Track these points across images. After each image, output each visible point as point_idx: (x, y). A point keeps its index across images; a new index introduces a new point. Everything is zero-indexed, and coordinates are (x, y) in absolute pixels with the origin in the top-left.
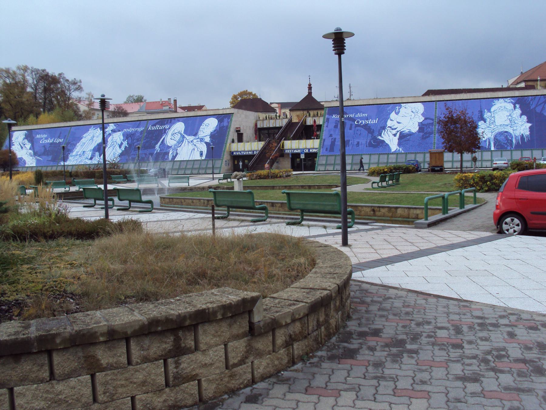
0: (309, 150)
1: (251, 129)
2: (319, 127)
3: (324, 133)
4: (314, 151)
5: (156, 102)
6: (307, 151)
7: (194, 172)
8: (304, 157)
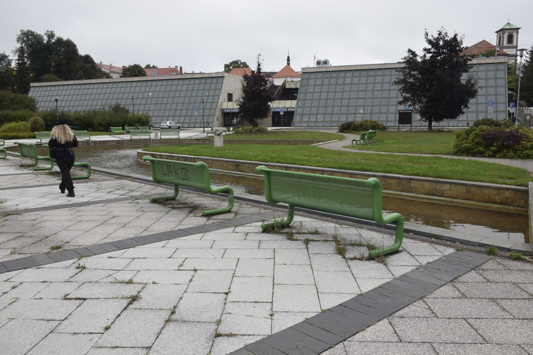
0: (287, 109)
3: (300, 96)
4: (292, 110)
6: (286, 110)
7: (191, 125)
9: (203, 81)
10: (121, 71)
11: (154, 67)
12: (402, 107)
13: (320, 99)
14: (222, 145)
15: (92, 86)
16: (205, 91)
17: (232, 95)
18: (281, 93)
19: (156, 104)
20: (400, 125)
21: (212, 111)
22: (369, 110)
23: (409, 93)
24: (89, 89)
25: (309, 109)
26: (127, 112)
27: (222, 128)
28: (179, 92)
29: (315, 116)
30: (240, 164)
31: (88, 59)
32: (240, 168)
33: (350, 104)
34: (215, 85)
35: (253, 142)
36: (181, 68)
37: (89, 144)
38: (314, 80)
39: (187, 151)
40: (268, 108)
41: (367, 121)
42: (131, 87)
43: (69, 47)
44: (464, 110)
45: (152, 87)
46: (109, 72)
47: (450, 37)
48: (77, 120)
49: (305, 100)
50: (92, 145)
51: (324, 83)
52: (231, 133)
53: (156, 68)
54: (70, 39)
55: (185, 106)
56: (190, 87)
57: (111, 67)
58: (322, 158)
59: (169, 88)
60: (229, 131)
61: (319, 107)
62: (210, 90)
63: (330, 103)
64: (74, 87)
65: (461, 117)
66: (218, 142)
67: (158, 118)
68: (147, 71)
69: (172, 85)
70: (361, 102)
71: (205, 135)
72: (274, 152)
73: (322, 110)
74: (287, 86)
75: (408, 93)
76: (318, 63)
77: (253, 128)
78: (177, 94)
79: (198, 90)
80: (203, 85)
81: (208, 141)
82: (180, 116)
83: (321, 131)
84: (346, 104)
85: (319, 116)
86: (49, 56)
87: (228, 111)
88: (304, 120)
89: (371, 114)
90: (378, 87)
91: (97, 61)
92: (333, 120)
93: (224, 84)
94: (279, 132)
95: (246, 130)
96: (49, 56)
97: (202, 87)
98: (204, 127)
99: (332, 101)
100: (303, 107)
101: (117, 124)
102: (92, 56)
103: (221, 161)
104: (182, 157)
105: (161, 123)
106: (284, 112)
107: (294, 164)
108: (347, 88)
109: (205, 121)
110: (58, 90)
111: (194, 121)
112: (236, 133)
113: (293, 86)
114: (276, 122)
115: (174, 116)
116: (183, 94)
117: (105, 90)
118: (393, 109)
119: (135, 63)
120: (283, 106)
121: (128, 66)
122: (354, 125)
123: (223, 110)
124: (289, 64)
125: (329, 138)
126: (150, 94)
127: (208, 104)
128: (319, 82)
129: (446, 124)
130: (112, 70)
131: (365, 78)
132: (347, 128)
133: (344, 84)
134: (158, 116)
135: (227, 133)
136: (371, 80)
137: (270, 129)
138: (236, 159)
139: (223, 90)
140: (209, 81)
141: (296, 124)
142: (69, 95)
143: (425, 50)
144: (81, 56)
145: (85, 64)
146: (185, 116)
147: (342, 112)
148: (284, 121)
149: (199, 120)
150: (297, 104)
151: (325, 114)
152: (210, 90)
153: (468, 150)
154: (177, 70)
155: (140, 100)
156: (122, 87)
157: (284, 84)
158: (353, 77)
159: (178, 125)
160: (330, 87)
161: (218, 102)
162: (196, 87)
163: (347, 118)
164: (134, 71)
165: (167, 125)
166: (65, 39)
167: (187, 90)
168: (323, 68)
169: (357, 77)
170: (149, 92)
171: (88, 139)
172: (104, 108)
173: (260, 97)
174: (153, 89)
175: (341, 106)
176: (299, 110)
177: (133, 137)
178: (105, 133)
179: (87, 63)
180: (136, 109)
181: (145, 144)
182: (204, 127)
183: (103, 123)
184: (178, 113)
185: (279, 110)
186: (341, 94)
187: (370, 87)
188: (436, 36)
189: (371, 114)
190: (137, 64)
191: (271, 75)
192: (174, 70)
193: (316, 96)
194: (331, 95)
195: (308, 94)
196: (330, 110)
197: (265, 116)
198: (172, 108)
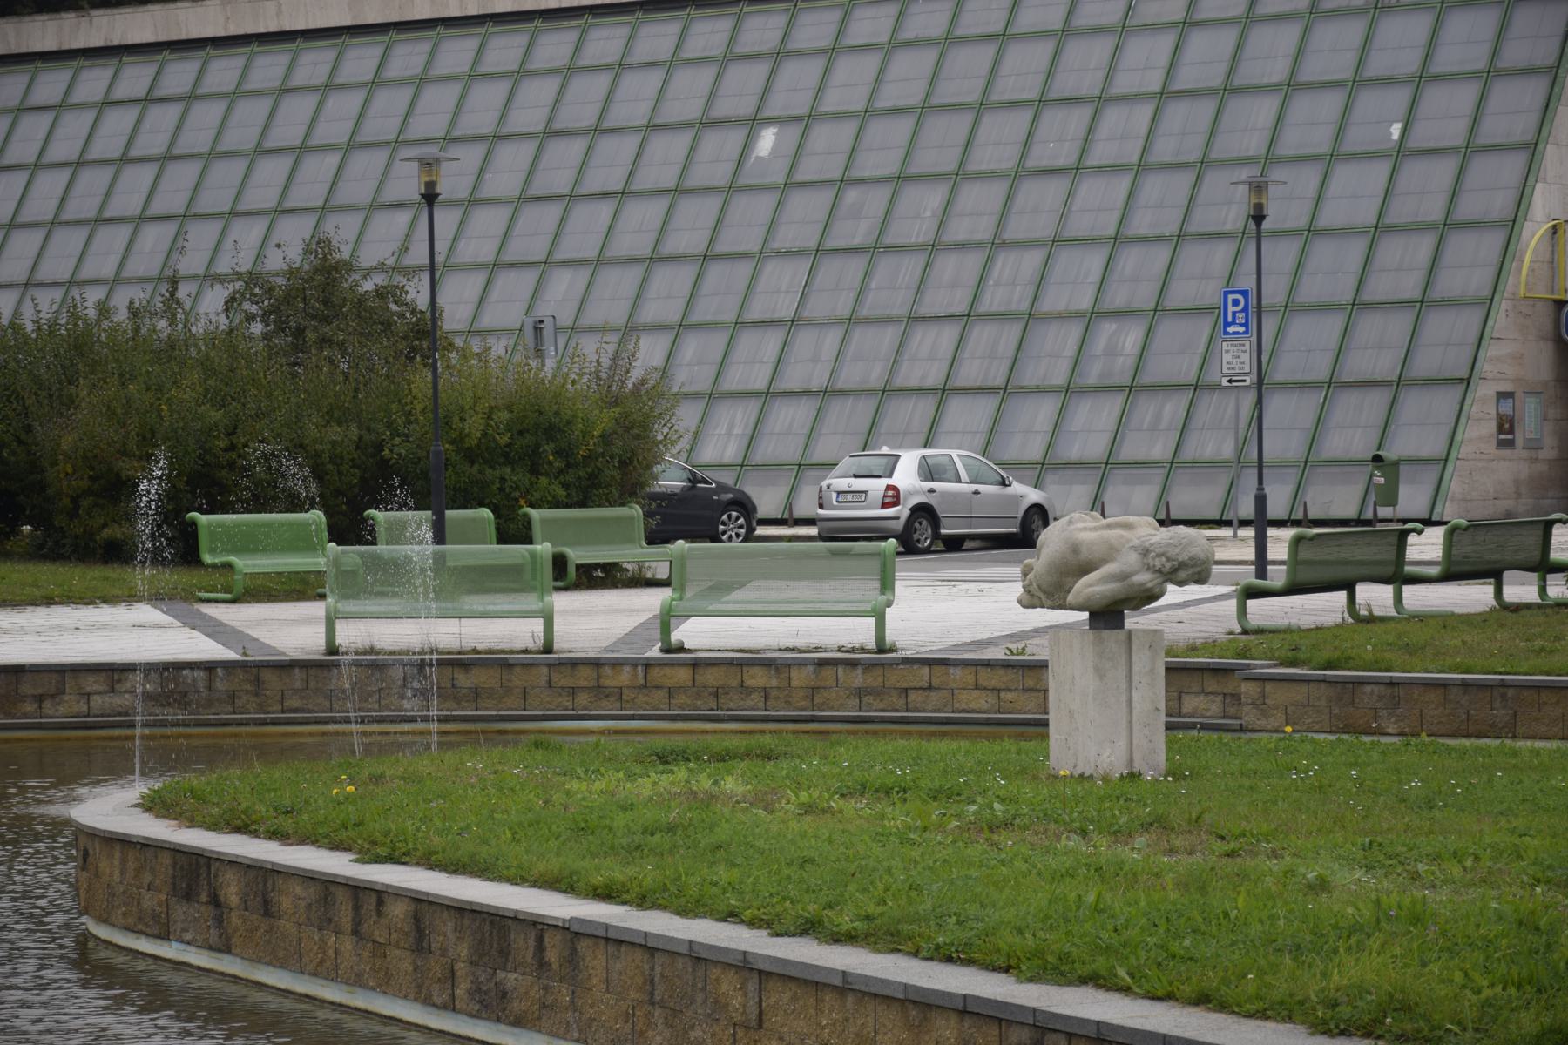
14: (1151, 750)
16: (1368, 102)
19: (820, 252)
26: (425, 335)
62: (1423, 79)
66: (1102, 725)
79: (1292, 86)
82: (1070, 391)
101: (435, 490)
104: (461, 910)
116: (1121, 132)
126: (767, 140)
134: (828, 393)
135: (1521, 589)
146: (1133, 389)
152: (1423, 79)
155: (931, 199)
161: (1512, 225)
165: (893, 497)
167: (1165, 95)
170: (755, 123)
177: (350, 635)
180: (512, 305)
184: (1052, 354)
198: (1181, 294)
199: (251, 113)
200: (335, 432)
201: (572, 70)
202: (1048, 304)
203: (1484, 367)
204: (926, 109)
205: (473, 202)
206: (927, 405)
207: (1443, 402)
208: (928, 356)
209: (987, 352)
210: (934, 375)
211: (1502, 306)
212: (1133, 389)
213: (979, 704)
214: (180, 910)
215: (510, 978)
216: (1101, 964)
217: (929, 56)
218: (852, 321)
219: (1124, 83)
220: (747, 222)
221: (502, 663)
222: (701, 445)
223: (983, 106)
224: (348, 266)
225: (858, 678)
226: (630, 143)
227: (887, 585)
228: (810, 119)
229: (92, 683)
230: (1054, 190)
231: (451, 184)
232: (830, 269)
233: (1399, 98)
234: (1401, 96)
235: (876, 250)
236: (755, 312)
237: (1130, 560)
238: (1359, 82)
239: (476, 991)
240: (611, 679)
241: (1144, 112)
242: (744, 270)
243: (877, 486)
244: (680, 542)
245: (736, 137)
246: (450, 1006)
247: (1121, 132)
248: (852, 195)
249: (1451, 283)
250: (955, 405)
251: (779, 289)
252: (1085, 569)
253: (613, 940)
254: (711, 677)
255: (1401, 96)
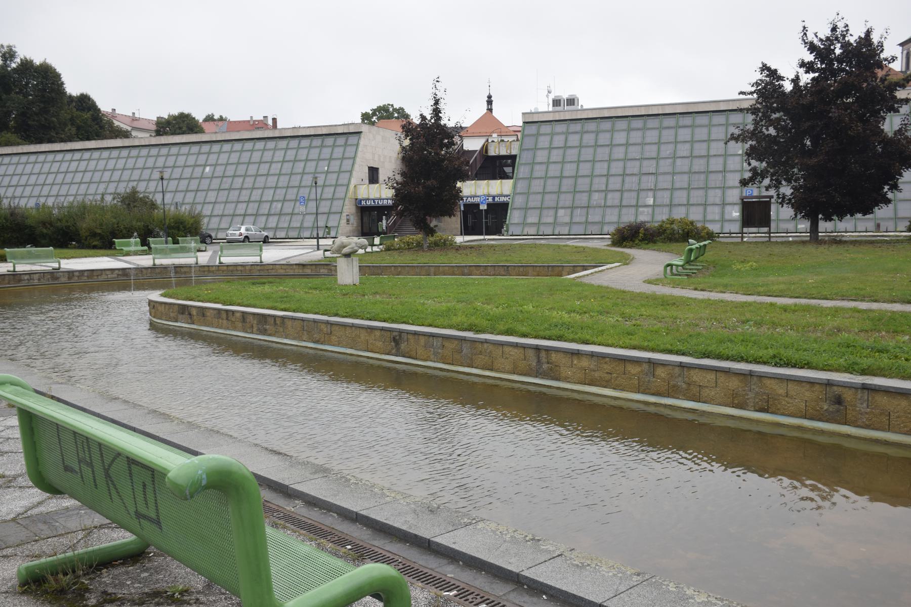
0: (494, 198)
1: (393, 161)
2: (513, 158)
3: (522, 170)
4: (502, 199)
5: (244, 122)
6: (490, 199)
7: (291, 234)
8: (485, 207)
9: (317, 142)
10: (154, 128)
11: (221, 119)
12: (753, 191)
13: (561, 177)
14: (357, 280)
15: (87, 155)
16: (321, 163)
17: (377, 169)
18: (479, 166)
20: (745, 230)
21: (335, 203)
22: (665, 197)
23: (761, 161)
24: (80, 160)
25: (539, 197)
26: (153, 205)
27: (356, 239)
28: (267, 165)
29: (552, 212)
30: (404, 336)
31: (85, 102)
32: (403, 346)
33: (627, 187)
34: (341, 149)
35: (426, 270)
36: (274, 120)
37: (57, 278)
38: (548, 138)
39: (268, 298)
40: (456, 195)
41: (672, 222)
42: (168, 155)
43: (47, 77)
44: (890, 195)
45: (211, 156)
46: (129, 129)
47: (856, 37)
48: (44, 223)
49: (531, 178)
50: (64, 279)
51: (569, 144)
52: (375, 249)
53: (225, 120)
54: (49, 61)
55: (280, 194)
56: (291, 155)
57: (134, 119)
58: (623, 315)
59: (245, 157)
60: (373, 245)
61: (559, 192)
62: (331, 159)
63: (583, 184)
64: (50, 157)
65: (882, 212)
66: (347, 274)
67: (224, 219)
68: (207, 127)
69: (252, 151)
70: (648, 182)
71: (319, 255)
72: (489, 300)
73: (566, 200)
74: (492, 152)
75: (761, 160)
76: (556, 102)
77: (425, 239)
78: (264, 169)
79: (307, 160)
80: (318, 150)
81: (325, 268)
82: (268, 215)
83: (570, 243)
84: (618, 187)
85: (561, 212)
86: (4, 96)
87: (368, 203)
88: (529, 220)
89: (671, 206)
90: (684, 150)
91: (104, 106)
92: (590, 219)
93: (360, 149)
94: (480, 246)
95: (408, 244)
96: (4, 96)
97: (314, 153)
98: (318, 238)
99: (588, 180)
100: (528, 194)
102: (94, 96)
103: (353, 326)
104: (254, 314)
105: (228, 229)
106: (488, 205)
107: (560, 338)
108: (619, 153)
109: (321, 223)
110: (18, 164)
111: (298, 225)
112: (388, 249)
113: (503, 152)
114: (470, 224)
115: (256, 215)
116: (275, 168)
117: (114, 161)
118: (734, 195)
119: (181, 111)
120: (485, 192)
121: (166, 117)
122: (646, 230)
123: (358, 201)
124: (490, 110)
125: (597, 260)
126: (208, 169)
127: (327, 190)
128: (559, 141)
129: (851, 226)
130: (136, 124)
131: (655, 133)
132: (631, 236)
133: (611, 145)
134: (222, 216)
135: (369, 249)
136: (668, 135)
137: (459, 239)
138: (393, 322)
139: (358, 160)
140: (329, 141)
141: (512, 229)
142: (39, 174)
143: (803, 64)
144: (70, 96)
145: (79, 113)
146: (280, 215)
147: (609, 203)
148: (486, 223)
149: (309, 221)
150: (515, 186)
151: (573, 208)
152: (331, 159)
153: (444, 243)
154: (266, 125)
155: (185, 182)
156: (148, 156)
157: (485, 148)
158: (629, 130)
159: (266, 234)
160: (583, 150)
161: (348, 185)
162: (303, 154)
163: (620, 216)
164: (180, 124)
165: (241, 234)
166: (37, 61)
167: (283, 162)
168: (567, 113)
169: (639, 129)
170: (205, 166)
171: (56, 265)
172: (102, 199)
173: (435, 178)
174: (213, 159)
175: (607, 191)
176: (519, 201)
177: (158, 262)
178: (102, 251)
179: (83, 110)
180: (173, 199)
181: (181, 276)
182: (318, 238)
183: (99, 231)
184: (265, 208)
185: (477, 200)
186: (606, 165)
187: (667, 150)
188: (825, 32)
189: (671, 206)
190: (186, 112)
191: (459, 129)
192: (261, 125)
193: (554, 170)
194: (585, 169)
195: (537, 167)
196: (582, 199)
197: (450, 214)
199: (20, 167)
200: (139, 224)
201: (118, 158)
202: (263, 199)
203: (344, 210)
204: (238, 163)
205: (170, 179)
206: (241, 218)
207: (337, 217)
208: (241, 209)
209: (253, 208)
210: (243, 212)
211: (347, 199)
212: (280, 215)
213: (282, 272)
214: (180, 316)
215: (268, 327)
216: (405, 319)
217: (238, 154)
218: (226, 202)
219: (275, 159)
220: (205, 184)
221: (189, 267)
222: (209, 225)
223: (249, 163)
224: (138, 192)
225: (259, 268)
226: (180, 169)
227: (261, 250)
228: (216, 165)
229: (108, 273)
230: (263, 178)
231: (166, 176)
232: (221, 193)
233: (327, 162)
234: (327, 162)
235: (230, 189)
236: (207, 201)
237: (354, 245)
238: (319, 160)
239: (258, 329)
240: (211, 269)
241: (280, 165)
242: (204, 193)
243: (238, 233)
244: (51, 248)
245: (202, 168)
246: (252, 333)
247: (275, 168)
248: (225, 179)
249: (337, 195)
250: (247, 218)
251: (212, 196)
252: (345, 247)
253: (293, 319)
254: (231, 268)
255: (327, 162)
